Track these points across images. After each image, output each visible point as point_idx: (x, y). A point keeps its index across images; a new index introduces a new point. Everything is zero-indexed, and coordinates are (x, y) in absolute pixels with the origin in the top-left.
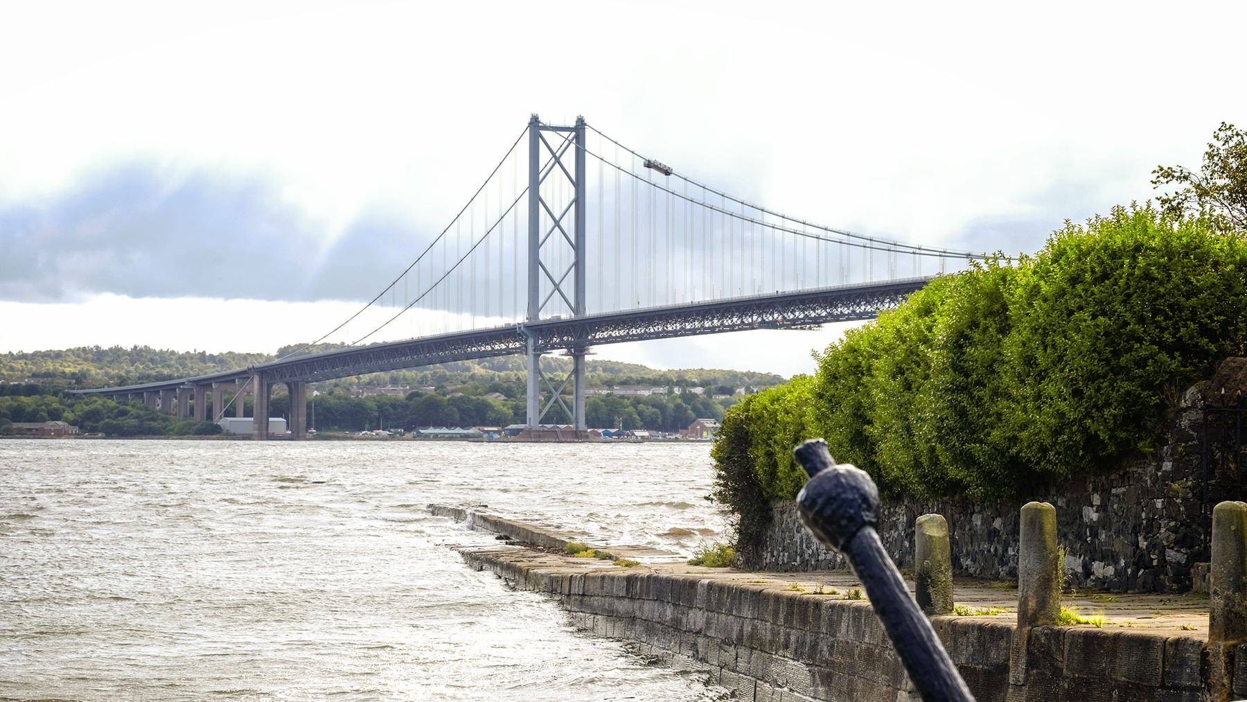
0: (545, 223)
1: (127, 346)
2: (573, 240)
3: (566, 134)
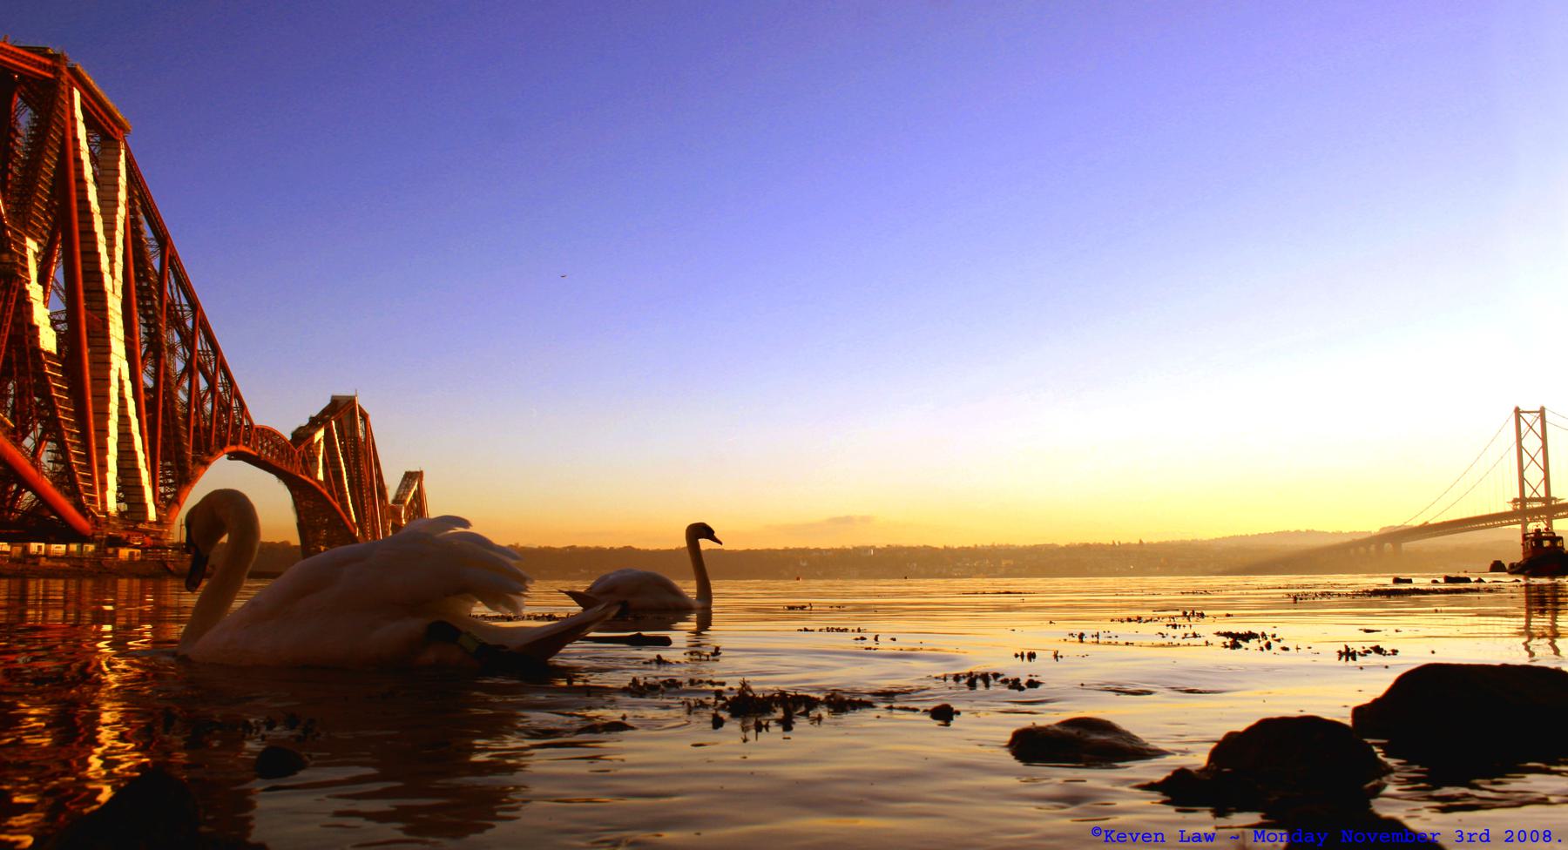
0: (1526, 459)
1: (1303, 529)
2: (1525, 483)
3: (1535, 414)
